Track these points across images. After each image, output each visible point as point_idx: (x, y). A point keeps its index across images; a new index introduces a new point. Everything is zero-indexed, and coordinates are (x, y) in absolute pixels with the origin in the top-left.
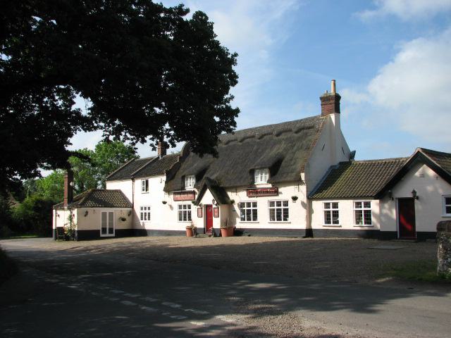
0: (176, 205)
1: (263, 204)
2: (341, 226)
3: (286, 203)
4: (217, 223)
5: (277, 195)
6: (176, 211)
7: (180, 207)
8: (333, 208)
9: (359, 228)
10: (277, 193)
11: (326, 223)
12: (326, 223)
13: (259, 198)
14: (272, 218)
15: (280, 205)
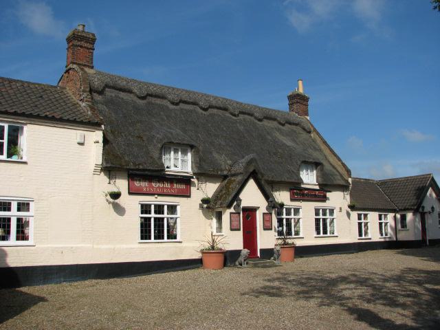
0: (132, 204)
1: (307, 210)
2: (370, 239)
3: (332, 212)
4: (266, 239)
5: (324, 201)
6: (134, 217)
7: (145, 209)
8: (156, 213)
9: (383, 240)
10: (324, 199)
11: (142, 239)
12: (142, 239)
13: (303, 203)
14: (145, 235)
15: (324, 214)
